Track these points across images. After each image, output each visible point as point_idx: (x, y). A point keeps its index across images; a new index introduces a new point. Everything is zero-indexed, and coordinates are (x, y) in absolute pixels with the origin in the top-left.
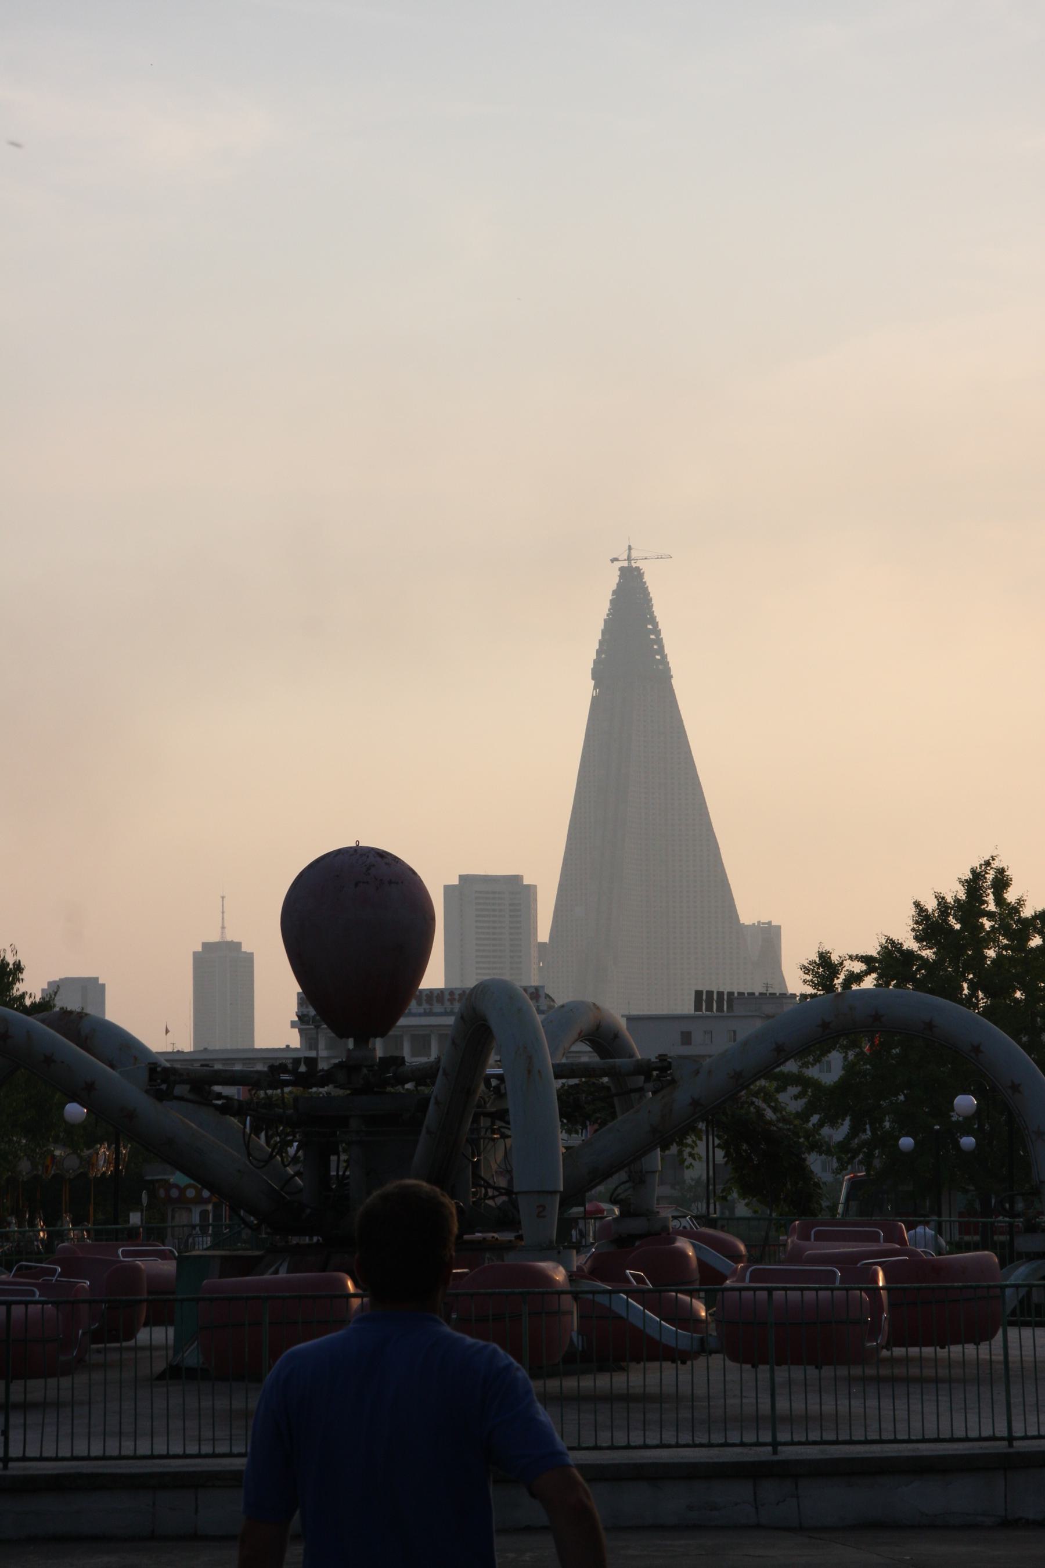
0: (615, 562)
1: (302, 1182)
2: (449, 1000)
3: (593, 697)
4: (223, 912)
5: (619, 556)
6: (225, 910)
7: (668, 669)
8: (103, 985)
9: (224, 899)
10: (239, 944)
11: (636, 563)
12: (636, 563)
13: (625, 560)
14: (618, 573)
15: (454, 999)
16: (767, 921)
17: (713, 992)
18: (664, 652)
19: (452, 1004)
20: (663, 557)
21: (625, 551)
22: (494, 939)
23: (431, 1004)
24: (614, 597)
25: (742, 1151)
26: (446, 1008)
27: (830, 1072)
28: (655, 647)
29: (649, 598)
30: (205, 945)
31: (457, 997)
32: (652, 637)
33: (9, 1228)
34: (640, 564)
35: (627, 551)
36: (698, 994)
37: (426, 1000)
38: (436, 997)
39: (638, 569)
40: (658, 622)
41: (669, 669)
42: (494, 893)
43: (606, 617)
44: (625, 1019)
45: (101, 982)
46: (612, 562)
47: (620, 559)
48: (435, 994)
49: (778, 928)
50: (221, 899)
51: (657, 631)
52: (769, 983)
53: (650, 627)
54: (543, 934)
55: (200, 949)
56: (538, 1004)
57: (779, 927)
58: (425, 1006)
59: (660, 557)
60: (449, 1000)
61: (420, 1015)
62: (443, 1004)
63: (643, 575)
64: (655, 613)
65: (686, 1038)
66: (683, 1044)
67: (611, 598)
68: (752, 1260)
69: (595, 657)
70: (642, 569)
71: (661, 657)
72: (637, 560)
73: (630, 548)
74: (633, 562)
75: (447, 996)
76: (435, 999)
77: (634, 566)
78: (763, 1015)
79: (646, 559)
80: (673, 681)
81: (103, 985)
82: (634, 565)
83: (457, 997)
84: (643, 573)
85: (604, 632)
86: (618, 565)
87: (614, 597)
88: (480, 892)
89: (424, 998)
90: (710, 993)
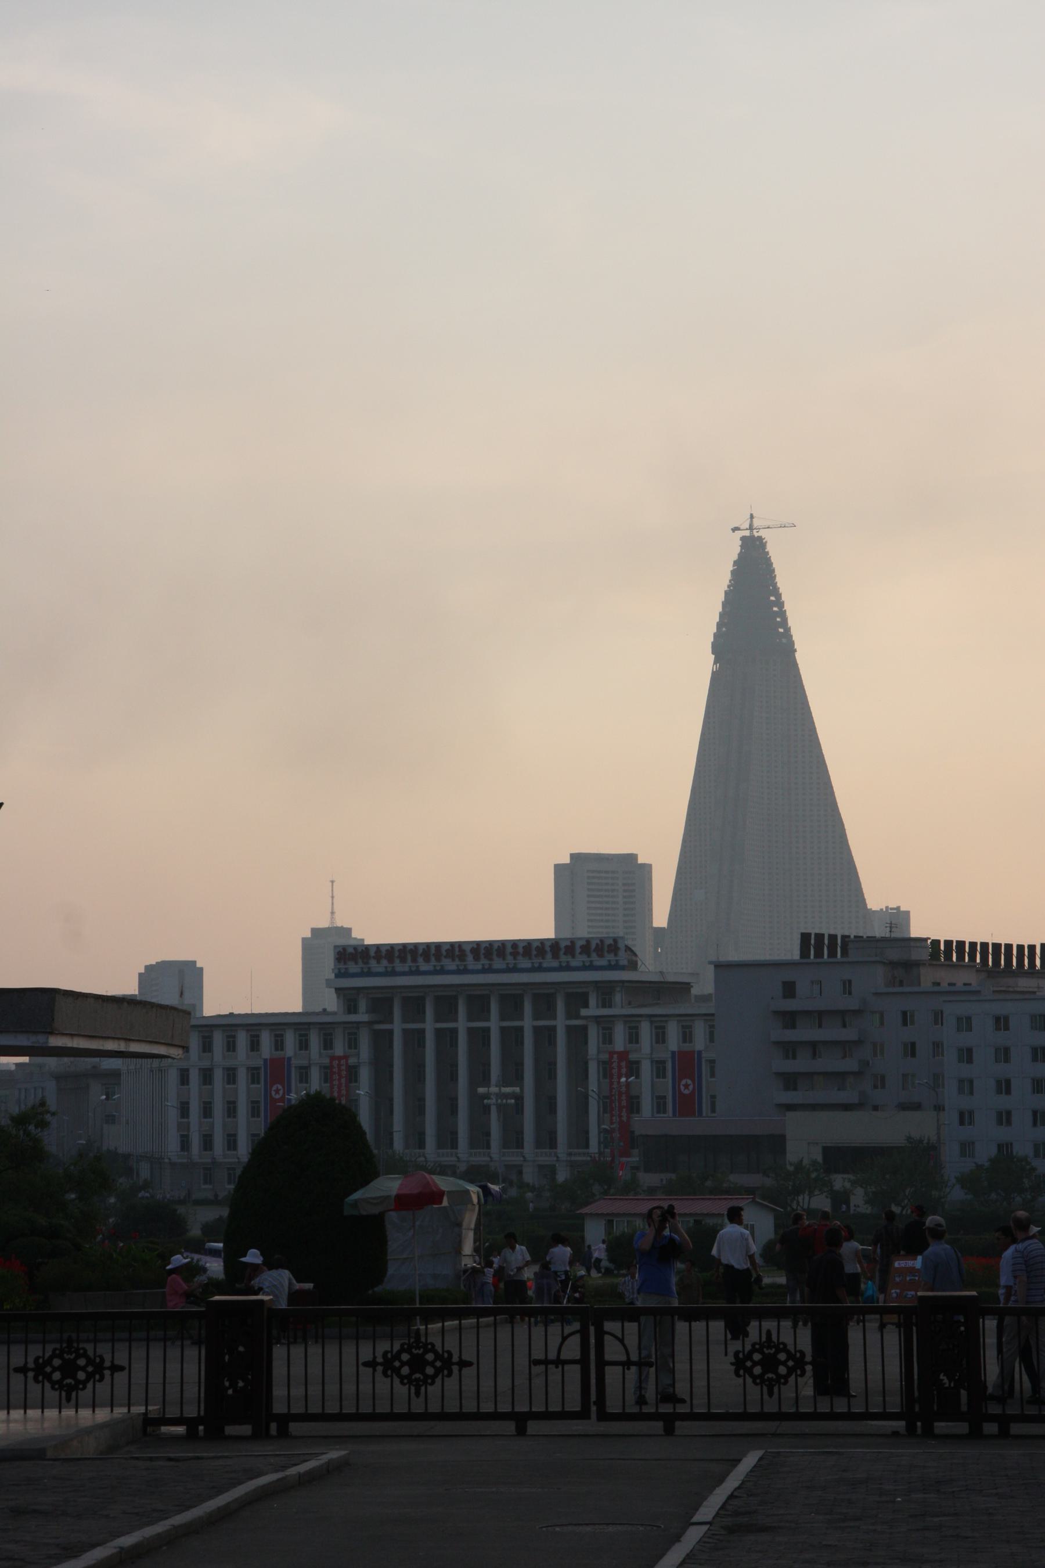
0: (736, 532)
1: (782, 1208)
2: (511, 954)
3: (713, 673)
4: (333, 897)
5: (741, 525)
6: (335, 894)
7: (791, 643)
8: (201, 969)
9: (334, 884)
10: (350, 930)
11: (757, 532)
12: (757, 532)
13: (747, 529)
14: (740, 543)
15: (518, 953)
16: (895, 907)
18: (794, 647)
19: (515, 959)
20: (786, 525)
21: (748, 519)
22: (607, 921)
23: (491, 959)
24: (736, 567)
26: (508, 964)
27: (971, 1031)
28: (778, 619)
29: (772, 568)
30: (314, 931)
31: (521, 950)
32: (775, 609)
34: (762, 533)
35: (749, 520)
36: (805, 937)
37: (484, 954)
38: (496, 950)
39: (760, 538)
41: (793, 643)
42: (607, 872)
44: (713, 966)
45: (198, 965)
46: (734, 532)
47: (742, 528)
48: (496, 946)
49: (907, 913)
50: (331, 883)
51: (780, 604)
52: (893, 922)
53: (772, 598)
54: (660, 917)
55: (309, 935)
56: (617, 958)
57: (908, 913)
58: (484, 961)
59: (783, 526)
60: (511, 954)
61: (477, 972)
62: (504, 959)
63: (766, 546)
64: (778, 584)
65: (789, 990)
66: (785, 997)
67: (732, 569)
69: (715, 630)
70: (764, 539)
72: (759, 529)
73: (752, 517)
74: (755, 531)
75: (509, 950)
76: (495, 953)
77: (756, 536)
78: (885, 961)
79: (768, 528)
80: (798, 655)
81: (201, 969)
82: (756, 534)
83: (521, 950)
84: (766, 542)
87: (736, 567)
88: (593, 871)
89: (483, 951)
90: (820, 937)
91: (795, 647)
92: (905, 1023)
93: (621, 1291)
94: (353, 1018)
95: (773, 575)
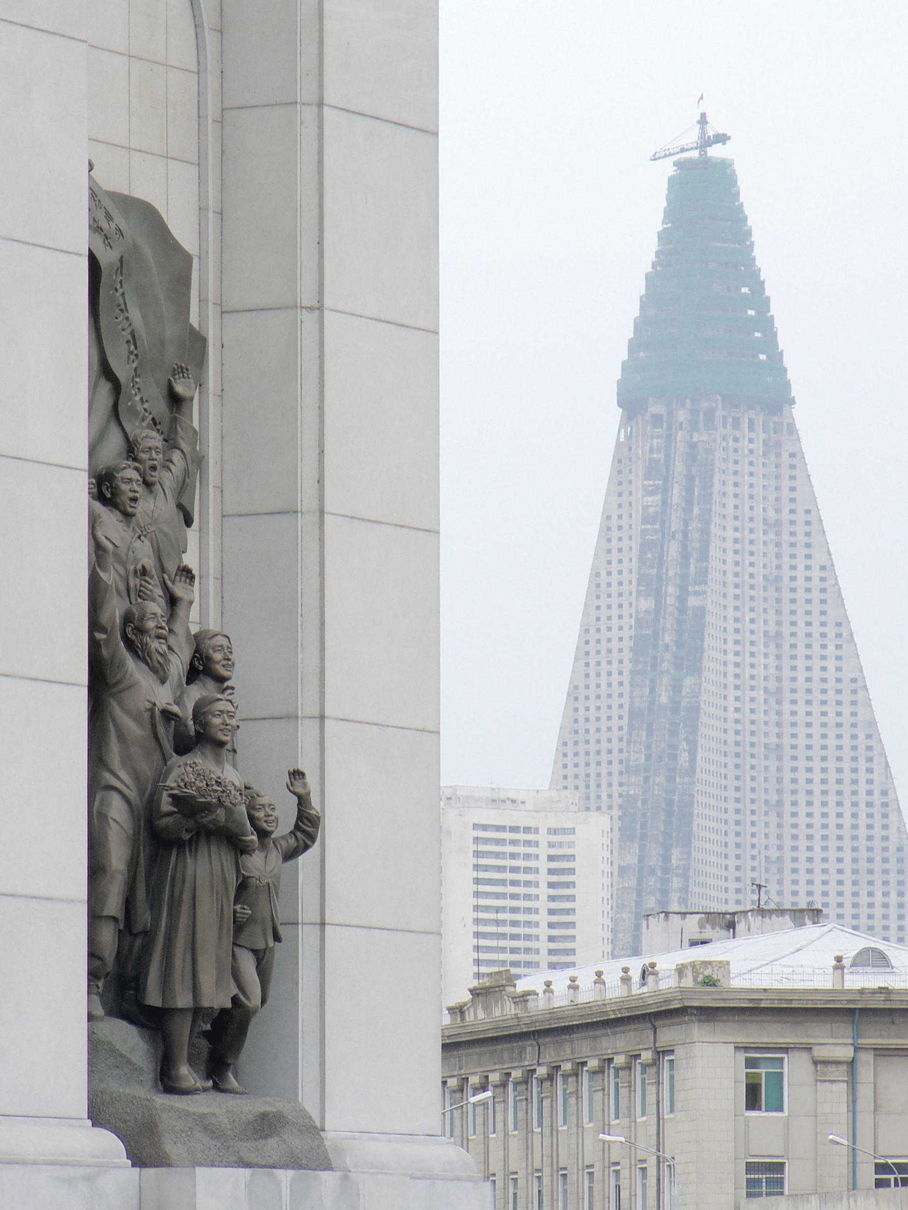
17: (902, 1186)
40: (763, 282)
43: (650, 269)
67: (661, 228)
69: (625, 356)
71: (768, 357)
85: (645, 303)
88: (485, 827)
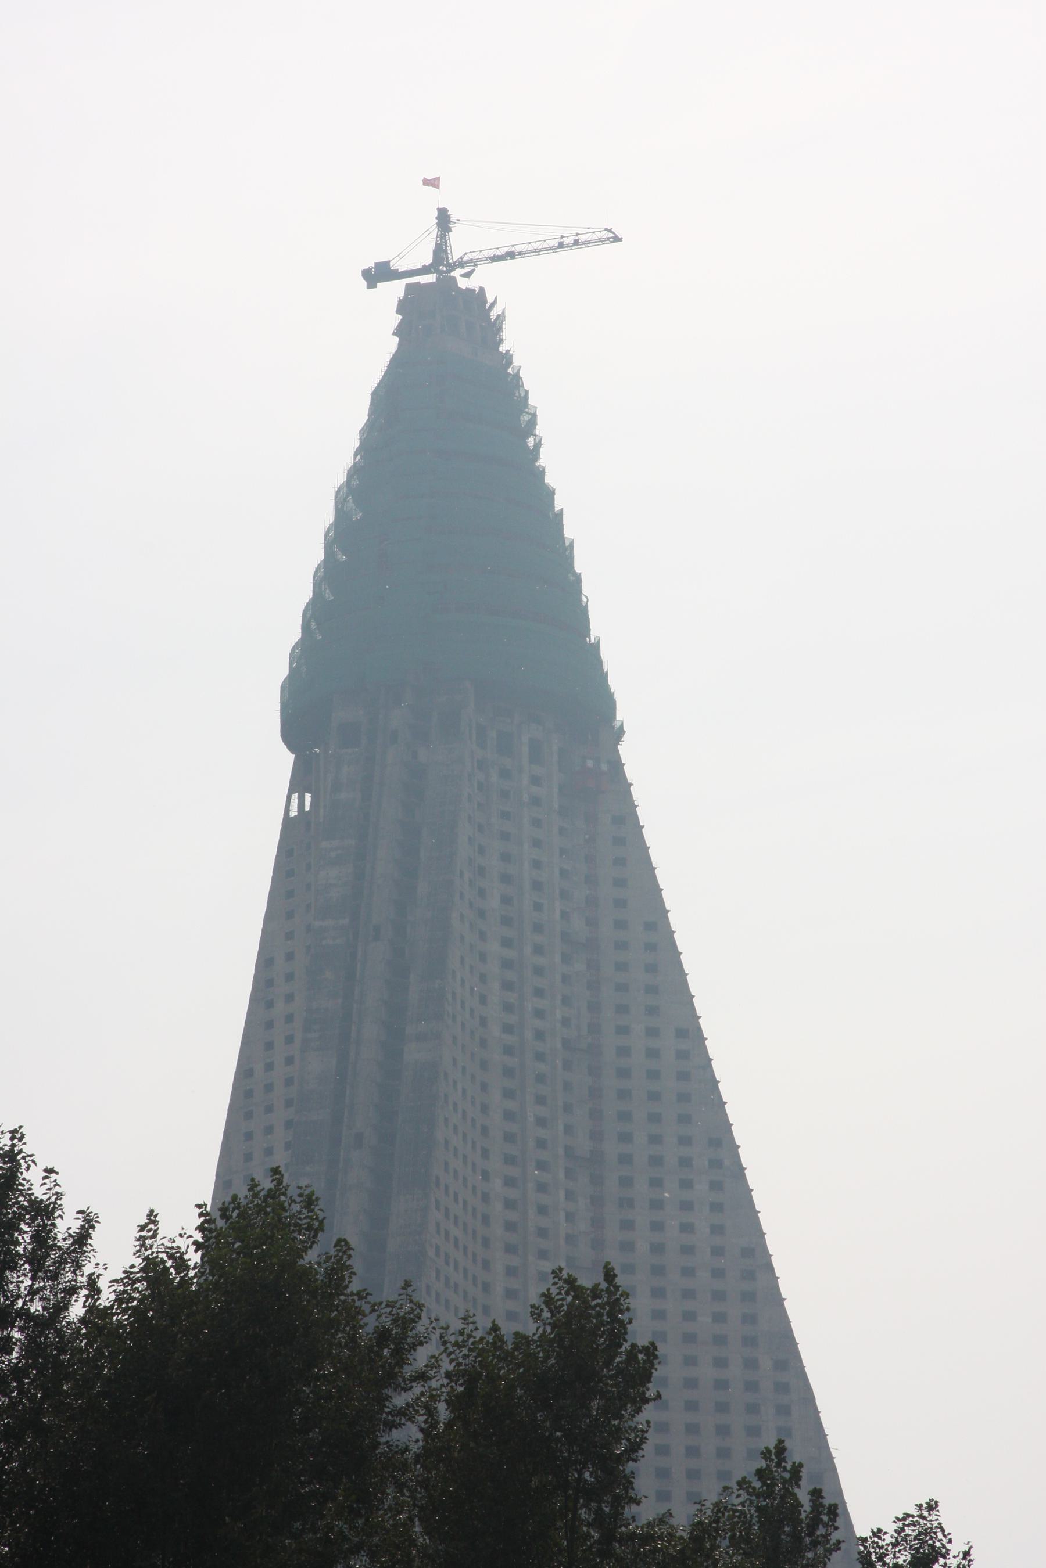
18: (587, 632)
20: (582, 238)
25: (604, 1302)
33: (599, 1284)
39: (477, 299)
63: (500, 329)
68: (629, 1415)
72: (475, 263)
73: (444, 220)
74: (457, 273)
79: (511, 255)
80: (626, 750)
84: (501, 318)
86: (395, 290)
91: (619, 717)
92: (427, 182)
93: (414, 1455)
94: (352, 1298)
95: (526, 418)
